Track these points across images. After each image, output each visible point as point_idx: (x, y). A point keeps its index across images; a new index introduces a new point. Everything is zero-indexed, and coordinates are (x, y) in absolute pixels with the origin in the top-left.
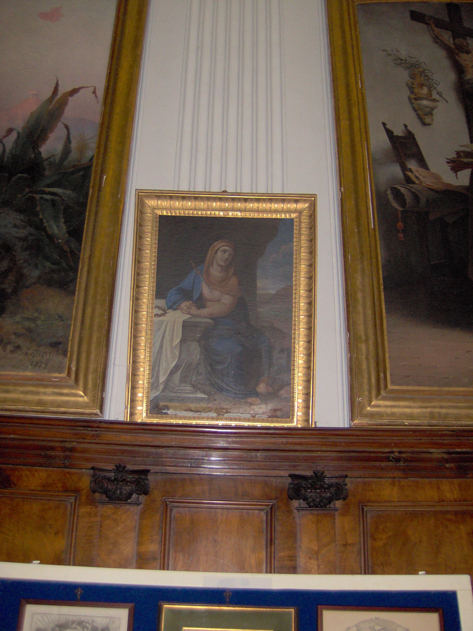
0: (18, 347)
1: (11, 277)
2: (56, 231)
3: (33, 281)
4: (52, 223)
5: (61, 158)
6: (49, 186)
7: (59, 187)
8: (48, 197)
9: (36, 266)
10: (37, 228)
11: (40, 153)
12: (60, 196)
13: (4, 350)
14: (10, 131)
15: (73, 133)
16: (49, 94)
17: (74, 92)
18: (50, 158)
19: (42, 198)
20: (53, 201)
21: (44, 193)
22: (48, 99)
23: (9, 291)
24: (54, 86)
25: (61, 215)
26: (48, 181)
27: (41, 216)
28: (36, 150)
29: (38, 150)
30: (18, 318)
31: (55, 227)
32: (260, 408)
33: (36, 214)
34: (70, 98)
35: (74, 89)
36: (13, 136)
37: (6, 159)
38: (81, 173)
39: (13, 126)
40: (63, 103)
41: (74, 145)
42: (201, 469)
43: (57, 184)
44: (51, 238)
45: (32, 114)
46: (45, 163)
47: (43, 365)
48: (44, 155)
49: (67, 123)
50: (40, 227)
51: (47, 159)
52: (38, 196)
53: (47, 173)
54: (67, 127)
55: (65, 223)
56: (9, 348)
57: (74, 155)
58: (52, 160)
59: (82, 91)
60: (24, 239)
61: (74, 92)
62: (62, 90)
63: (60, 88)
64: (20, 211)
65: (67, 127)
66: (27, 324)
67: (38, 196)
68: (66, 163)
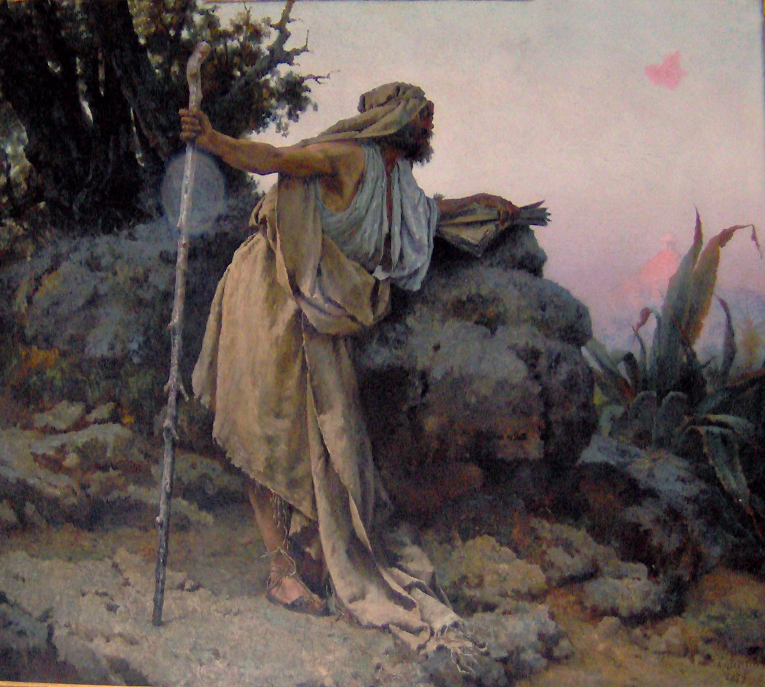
0: (708, 657)
1: (686, 559)
2: (734, 486)
3: (714, 563)
4: (727, 472)
5: (725, 362)
6: (715, 412)
7: (727, 412)
8: (716, 430)
9: (715, 541)
10: (707, 481)
11: (694, 355)
12: (732, 428)
13: (693, 661)
14: (646, 314)
15: (734, 314)
16: (690, 241)
17: (725, 236)
18: (709, 362)
19: (708, 432)
20: (722, 434)
21: (710, 423)
22: (690, 252)
23: (687, 578)
24: (695, 219)
25: (737, 460)
26: (712, 404)
27: (711, 462)
28: (688, 349)
29: (691, 349)
30: (702, 618)
31: (732, 478)
32: (228, 612)
33: (704, 458)
34: (722, 251)
35: (724, 230)
36: (652, 324)
37: (648, 367)
38: (755, 388)
39: (649, 304)
40: (713, 261)
41: (739, 338)
42: (307, 361)
43: (724, 408)
44: (730, 497)
45: (672, 280)
46: (704, 372)
47: (741, 679)
48: (701, 358)
49: (723, 298)
50: (710, 477)
51: (704, 366)
52: (702, 430)
53: (709, 389)
54: (724, 304)
55: (745, 471)
56: (698, 658)
57: (741, 357)
58: (712, 365)
59: (736, 234)
60: (694, 500)
61: (725, 236)
62: (711, 232)
63: (704, 230)
64: (683, 454)
65: (724, 304)
66: (714, 624)
67: (702, 430)
68: (732, 372)
